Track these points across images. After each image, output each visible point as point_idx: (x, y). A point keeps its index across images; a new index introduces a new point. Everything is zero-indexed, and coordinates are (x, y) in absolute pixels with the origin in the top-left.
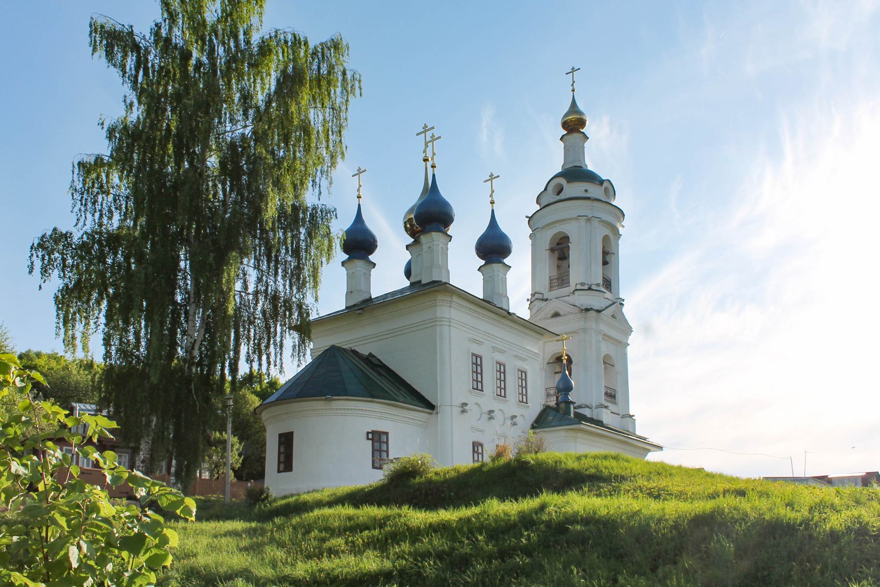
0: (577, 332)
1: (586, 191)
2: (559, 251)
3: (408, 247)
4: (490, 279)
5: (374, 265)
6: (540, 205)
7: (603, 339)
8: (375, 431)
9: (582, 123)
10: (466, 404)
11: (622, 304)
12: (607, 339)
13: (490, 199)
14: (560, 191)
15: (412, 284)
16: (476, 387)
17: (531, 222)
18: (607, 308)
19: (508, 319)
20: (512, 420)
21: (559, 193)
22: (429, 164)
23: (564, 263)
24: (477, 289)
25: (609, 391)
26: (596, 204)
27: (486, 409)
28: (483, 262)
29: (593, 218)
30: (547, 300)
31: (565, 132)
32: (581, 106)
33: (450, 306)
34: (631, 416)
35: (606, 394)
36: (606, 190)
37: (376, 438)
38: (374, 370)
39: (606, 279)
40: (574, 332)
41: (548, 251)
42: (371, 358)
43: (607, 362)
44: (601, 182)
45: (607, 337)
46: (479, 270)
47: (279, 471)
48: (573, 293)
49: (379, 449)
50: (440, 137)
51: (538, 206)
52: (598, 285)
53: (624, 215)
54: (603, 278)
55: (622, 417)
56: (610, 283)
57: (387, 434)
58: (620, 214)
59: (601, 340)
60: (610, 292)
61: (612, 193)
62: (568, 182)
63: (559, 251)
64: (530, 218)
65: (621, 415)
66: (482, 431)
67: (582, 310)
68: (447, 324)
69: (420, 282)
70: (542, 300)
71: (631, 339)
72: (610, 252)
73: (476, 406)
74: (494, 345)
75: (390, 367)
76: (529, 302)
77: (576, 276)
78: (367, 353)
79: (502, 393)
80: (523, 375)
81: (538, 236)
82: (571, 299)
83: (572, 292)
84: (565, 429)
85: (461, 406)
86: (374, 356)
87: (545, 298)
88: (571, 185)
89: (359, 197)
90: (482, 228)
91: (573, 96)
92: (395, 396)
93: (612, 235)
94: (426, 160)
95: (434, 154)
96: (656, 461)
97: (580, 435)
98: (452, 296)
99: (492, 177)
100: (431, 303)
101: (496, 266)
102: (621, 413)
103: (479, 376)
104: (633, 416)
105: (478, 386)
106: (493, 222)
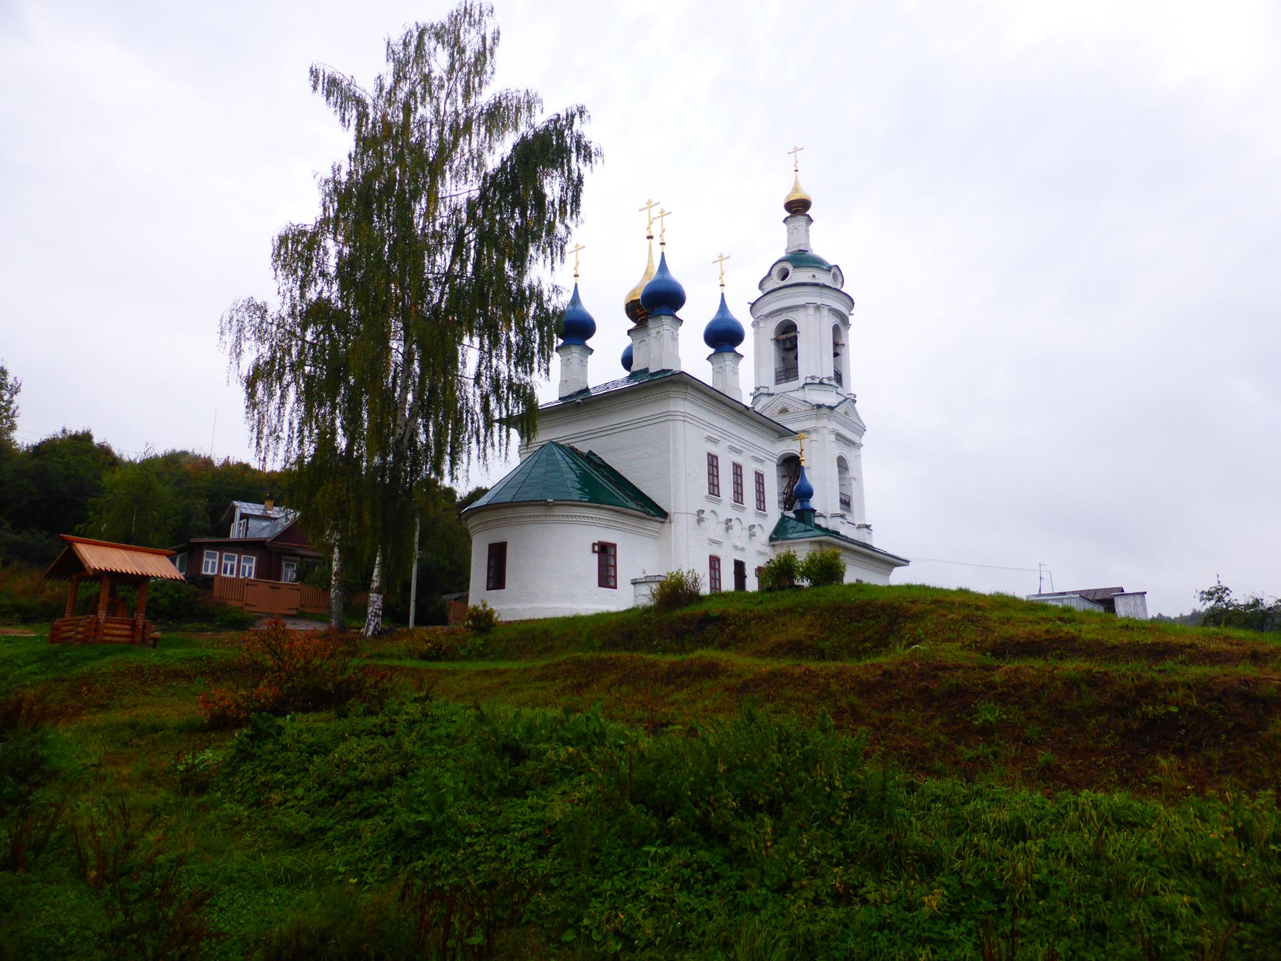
1: (814, 276)
3: (629, 332)
4: (721, 370)
5: (592, 351)
10: (703, 511)
11: (855, 401)
13: (719, 282)
14: (785, 275)
18: (840, 404)
19: (745, 415)
21: (784, 278)
22: (656, 241)
23: (791, 355)
26: (824, 291)
27: (723, 518)
28: (712, 351)
31: (788, 214)
34: (868, 527)
36: (835, 276)
42: (592, 457)
43: (842, 464)
44: (829, 269)
45: (839, 437)
46: (708, 359)
47: (488, 589)
50: (583, 247)
52: (829, 379)
53: (853, 303)
54: (835, 371)
57: (614, 546)
60: (841, 386)
64: (753, 305)
69: (646, 370)
71: (864, 440)
73: (712, 514)
77: (807, 366)
78: (586, 451)
79: (738, 495)
80: (759, 478)
81: (762, 324)
82: (799, 395)
83: (801, 386)
86: (595, 455)
88: (797, 270)
91: (797, 177)
92: (625, 502)
96: (993, 593)
99: (721, 258)
101: (728, 357)
102: (857, 523)
104: (870, 526)
105: (714, 488)
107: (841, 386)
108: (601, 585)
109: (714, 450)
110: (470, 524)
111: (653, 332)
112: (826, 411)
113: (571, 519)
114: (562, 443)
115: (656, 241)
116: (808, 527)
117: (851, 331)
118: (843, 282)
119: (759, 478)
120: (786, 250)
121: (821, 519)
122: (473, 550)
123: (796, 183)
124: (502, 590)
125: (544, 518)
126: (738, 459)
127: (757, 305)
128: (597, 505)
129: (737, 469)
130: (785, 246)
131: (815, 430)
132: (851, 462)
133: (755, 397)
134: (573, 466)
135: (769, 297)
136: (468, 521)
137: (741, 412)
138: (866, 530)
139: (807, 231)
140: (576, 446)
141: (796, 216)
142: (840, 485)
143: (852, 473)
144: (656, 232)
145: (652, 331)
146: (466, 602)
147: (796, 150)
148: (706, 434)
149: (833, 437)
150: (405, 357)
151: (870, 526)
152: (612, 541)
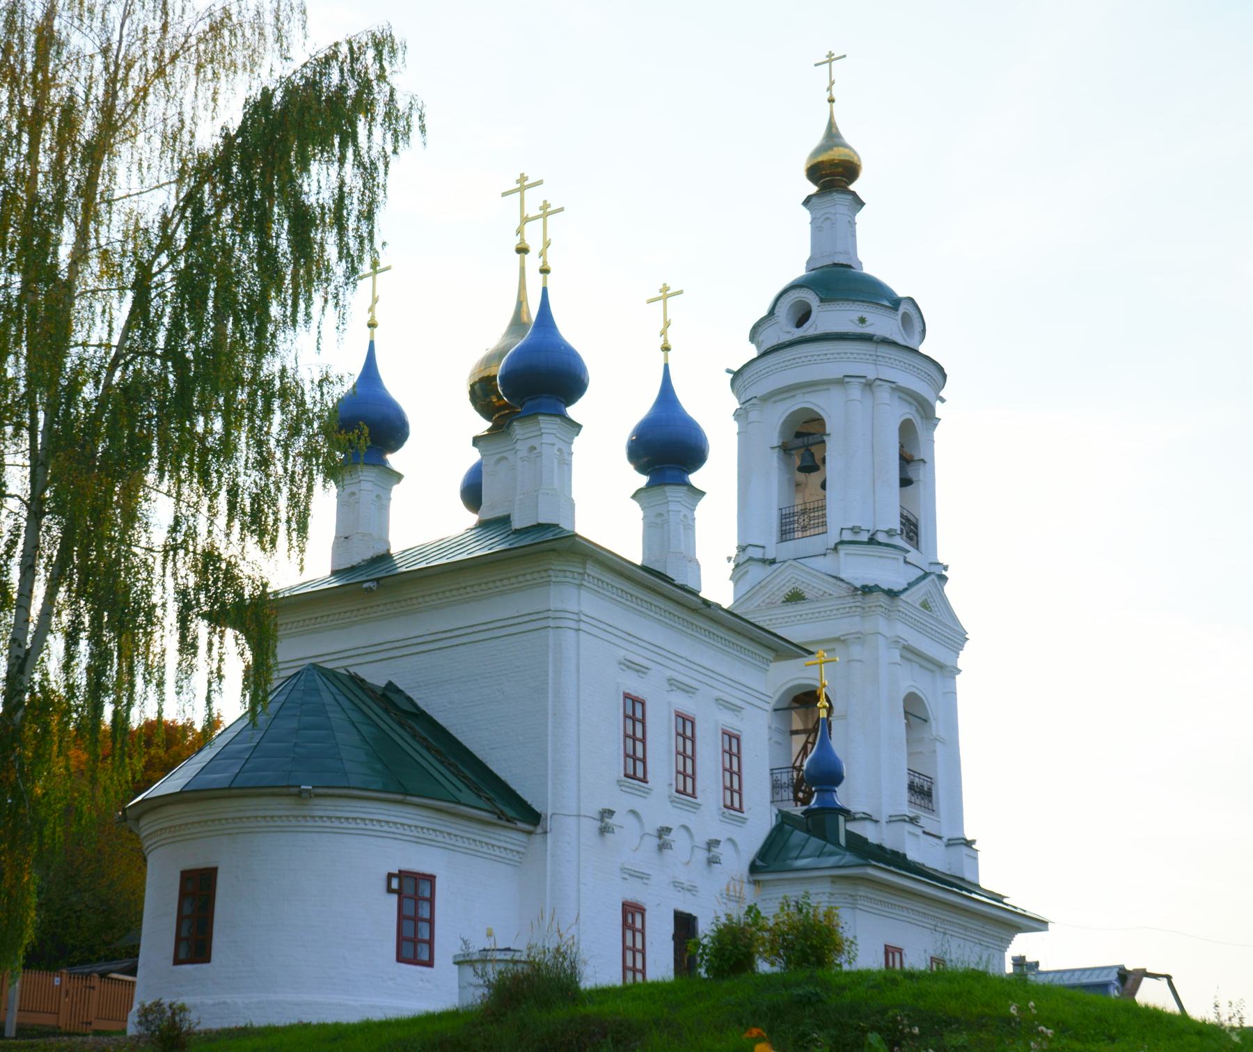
0: (844, 641)
1: (862, 320)
2: (802, 451)
3: (477, 441)
5: (398, 477)
6: (758, 347)
7: (902, 656)
8: (405, 872)
9: (849, 170)
10: (611, 813)
11: (943, 579)
12: (910, 656)
14: (803, 317)
15: (483, 525)
16: (682, 789)
17: (738, 383)
18: (910, 585)
20: (709, 850)
21: (800, 323)
22: (533, 262)
23: (814, 478)
24: (631, 548)
25: (917, 780)
26: (884, 350)
27: (652, 825)
28: (643, 480)
29: (847, 379)
30: (773, 562)
32: (848, 134)
33: (580, 586)
34: (969, 844)
35: (911, 787)
36: (906, 321)
37: (409, 890)
38: (401, 725)
39: (908, 520)
40: (837, 640)
41: (776, 450)
42: (393, 697)
44: (896, 303)
45: (910, 653)
46: (634, 497)
47: (177, 961)
48: (835, 549)
49: (412, 913)
51: (753, 347)
52: (890, 533)
53: (945, 376)
54: (902, 516)
55: (948, 845)
56: (916, 526)
57: (431, 879)
58: (938, 374)
59: (898, 659)
60: (917, 547)
61: (918, 328)
62: (822, 300)
63: (802, 451)
64: (737, 375)
65: (945, 840)
66: (642, 877)
67: (856, 589)
68: (573, 625)
69: (505, 521)
70: (764, 561)
71: (964, 660)
72: (916, 458)
74: (669, 673)
75: (435, 718)
76: (732, 565)
78: (381, 683)
81: (754, 415)
83: (833, 546)
84: (831, 876)
85: (598, 816)
86: (399, 691)
87: (770, 556)
88: (828, 307)
89: (372, 325)
90: (641, 406)
91: (831, 113)
93: (918, 418)
94: (522, 250)
95: (547, 244)
97: (862, 891)
98: (584, 564)
99: (666, 294)
100: (536, 575)
101: (673, 492)
102: (946, 834)
103: (639, 746)
104: (973, 842)
106: (667, 395)
107: (917, 547)
108: (400, 959)
109: (637, 687)
110: (146, 827)
111: (522, 447)
112: (883, 599)
113: (345, 825)
114: (329, 666)
115: (533, 262)
116: (830, 847)
117: (939, 434)
118: (924, 331)
119: (732, 740)
120: (808, 262)
121: (868, 824)
122: (149, 880)
123: (831, 126)
124: (204, 966)
125: (294, 823)
126: (687, 705)
127: (746, 375)
128: (400, 797)
129: (685, 723)
130: (806, 253)
131: (860, 638)
132: (934, 708)
133: (737, 566)
134: (356, 717)
135: (771, 359)
136: (142, 823)
137: (694, 610)
138: (965, 850)
139: (852, 224)
140: (363, 672)
141: (831, 192)
142: (910, 754)
143: (937, 727)
144: (533, 237)
145: (518, 446)
146: (126, 1033)
147: (831, 58)
148: (621, 654)
149: (896, 655)
150: (33, 508)
151: (973, 842)
152: (427, 870)
